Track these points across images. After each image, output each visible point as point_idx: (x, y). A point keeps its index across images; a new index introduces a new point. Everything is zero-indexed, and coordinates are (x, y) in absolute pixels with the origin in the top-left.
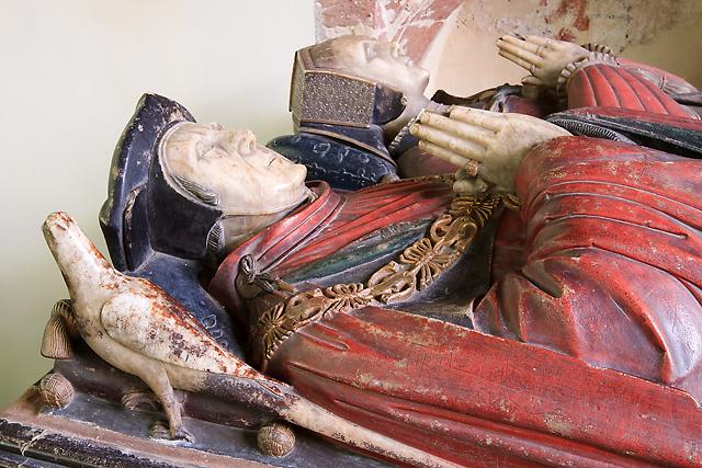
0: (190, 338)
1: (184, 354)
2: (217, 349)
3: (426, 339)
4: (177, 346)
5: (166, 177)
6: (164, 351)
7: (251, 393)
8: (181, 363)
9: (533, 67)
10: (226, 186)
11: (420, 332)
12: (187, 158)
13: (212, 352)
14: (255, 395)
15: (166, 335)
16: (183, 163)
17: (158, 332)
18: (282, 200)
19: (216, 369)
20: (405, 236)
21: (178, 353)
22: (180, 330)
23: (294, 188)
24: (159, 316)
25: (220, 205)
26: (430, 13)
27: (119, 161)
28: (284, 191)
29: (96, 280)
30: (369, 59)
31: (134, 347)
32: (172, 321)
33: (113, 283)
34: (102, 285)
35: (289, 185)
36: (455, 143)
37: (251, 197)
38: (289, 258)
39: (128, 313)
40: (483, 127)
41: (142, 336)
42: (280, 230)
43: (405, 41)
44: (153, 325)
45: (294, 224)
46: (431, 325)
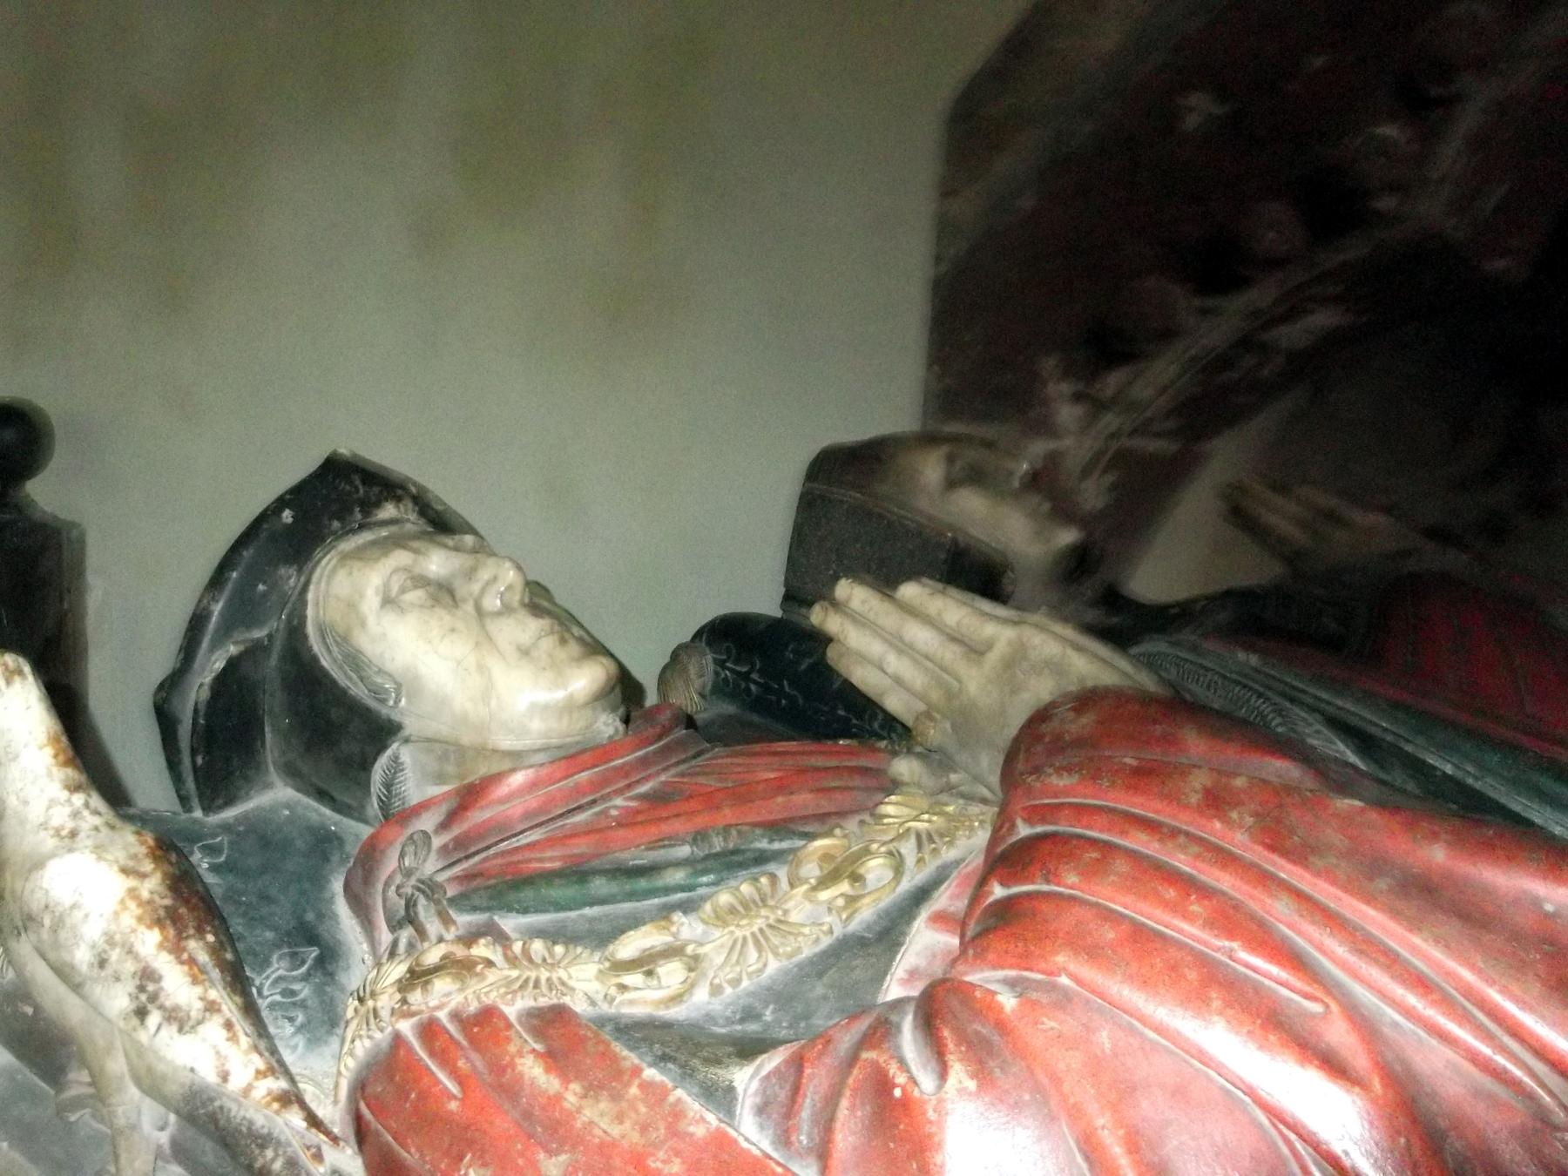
0: (178, 986)
1: (154, 1018)
2: (229, 1025)
3: (620, 1118)
4: (143, 997)
5: (311, 629)
6: (118, 1000)
7: (263, 1147)
8: (143, 1037)
9: (1293, 558)
11: (616, 1097)
12: (362, 596)
13: (213, 1029)
14: (269, 1153)
15: (130, 967)
16: (352, 606)
17: (115, 955)
18: (537, 725)
19: (209, 1075)
20: (735, 858)
21: (141, 1013)
22: (165, 964)
23: (569, 707)
24: (128, 920)
25: (407, 713)
26: (1171, 424)
27: (216, 581)
28: (546, 708)
29: (35, 813)
30: (951, 484)
31: (64, 972)
32: (155, 936)
33: (70, 825)
34: (44, 826)
35: (560, 695)
36: (894, 663)
37: (469, 706)
38: (496, 856)
39: (67, 903)
40: (954, 638)
41: (82, 957)
42: (502, 790)
43: (1110, 478)
44: (111, 941)
45: (1284, 872)
46: (646, 1086)
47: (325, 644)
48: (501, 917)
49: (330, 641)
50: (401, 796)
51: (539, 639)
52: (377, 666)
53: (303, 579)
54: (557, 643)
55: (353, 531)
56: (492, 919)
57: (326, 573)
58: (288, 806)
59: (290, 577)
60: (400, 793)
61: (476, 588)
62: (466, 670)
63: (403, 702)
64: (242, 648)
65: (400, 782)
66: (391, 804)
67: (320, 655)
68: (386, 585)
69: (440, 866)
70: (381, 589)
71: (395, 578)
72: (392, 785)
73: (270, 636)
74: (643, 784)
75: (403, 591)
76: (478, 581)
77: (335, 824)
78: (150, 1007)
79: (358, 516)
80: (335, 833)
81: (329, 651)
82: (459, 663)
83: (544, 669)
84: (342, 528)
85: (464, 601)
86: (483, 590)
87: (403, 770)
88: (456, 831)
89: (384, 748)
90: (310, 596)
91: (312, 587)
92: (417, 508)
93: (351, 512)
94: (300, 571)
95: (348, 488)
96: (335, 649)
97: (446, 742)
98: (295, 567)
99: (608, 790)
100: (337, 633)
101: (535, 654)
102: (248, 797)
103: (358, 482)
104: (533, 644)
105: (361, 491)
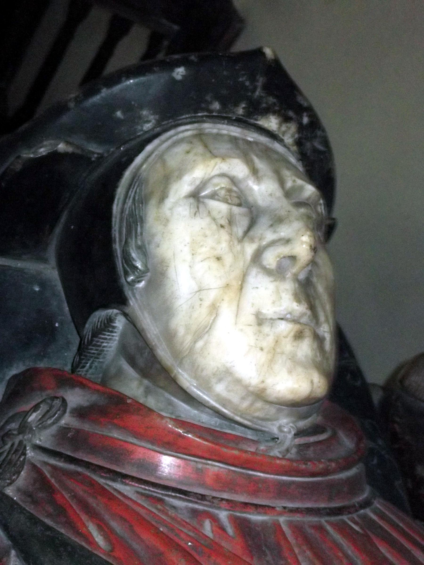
5: (128, 174)
10: (171, 273)
12: (180, 177)
37: (181, 331)
47: (127, 192)
48: (17, 556)
49: (132, 194)
50: (100, 348)
51: (282, 319)
52: (143, 242)
53: (158, 129)
54: (292, 334)
55: (231, 121)
56: (7, 553)
57: (175, 138)
58: (43, 284)
59: (148, 122)
60: (100, 346)
61: (270, 236)
62: (201, 300)
63: (142, 285)
64: (70, 149)
65: (106, 339)
66: (88, 349)
67: (116, 200)
68: (204, 184)
69: (47, 445)
70: (198, 182)
71: (216, 181)
72: (96, 337)
73: (101, 157)
74: (259, 513)
75: (213, 196)
76: (275, 232)
77: (61, 323)
78: (256, 240)
79: (240, 111)
80: (54, 329)
81: (124, 202)
82: (200, 290)
83: (262, 349)
84: (219, 111)
85: (252, 240)
86: (273, 243)
87: (112, 332)
88: (87, 427)
89: (106, 306)
90: (149, 148)
91: (156, 142)
92: (297, 136)
93: (236, 105)
94: (158, 123)
95: (247, 83)
96: (130, 202)
97: (148, 345)
98: (157, 117)
99: (225, 496)
100: (141, 190)
101: (266, 329)
102: (18, 257)
103: (261, 81)
104: (271, 319)
105: (257, 93)
